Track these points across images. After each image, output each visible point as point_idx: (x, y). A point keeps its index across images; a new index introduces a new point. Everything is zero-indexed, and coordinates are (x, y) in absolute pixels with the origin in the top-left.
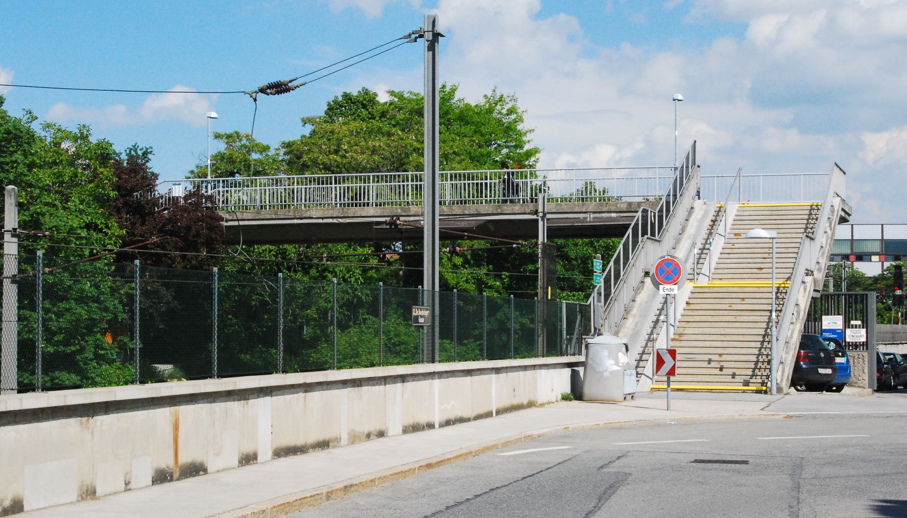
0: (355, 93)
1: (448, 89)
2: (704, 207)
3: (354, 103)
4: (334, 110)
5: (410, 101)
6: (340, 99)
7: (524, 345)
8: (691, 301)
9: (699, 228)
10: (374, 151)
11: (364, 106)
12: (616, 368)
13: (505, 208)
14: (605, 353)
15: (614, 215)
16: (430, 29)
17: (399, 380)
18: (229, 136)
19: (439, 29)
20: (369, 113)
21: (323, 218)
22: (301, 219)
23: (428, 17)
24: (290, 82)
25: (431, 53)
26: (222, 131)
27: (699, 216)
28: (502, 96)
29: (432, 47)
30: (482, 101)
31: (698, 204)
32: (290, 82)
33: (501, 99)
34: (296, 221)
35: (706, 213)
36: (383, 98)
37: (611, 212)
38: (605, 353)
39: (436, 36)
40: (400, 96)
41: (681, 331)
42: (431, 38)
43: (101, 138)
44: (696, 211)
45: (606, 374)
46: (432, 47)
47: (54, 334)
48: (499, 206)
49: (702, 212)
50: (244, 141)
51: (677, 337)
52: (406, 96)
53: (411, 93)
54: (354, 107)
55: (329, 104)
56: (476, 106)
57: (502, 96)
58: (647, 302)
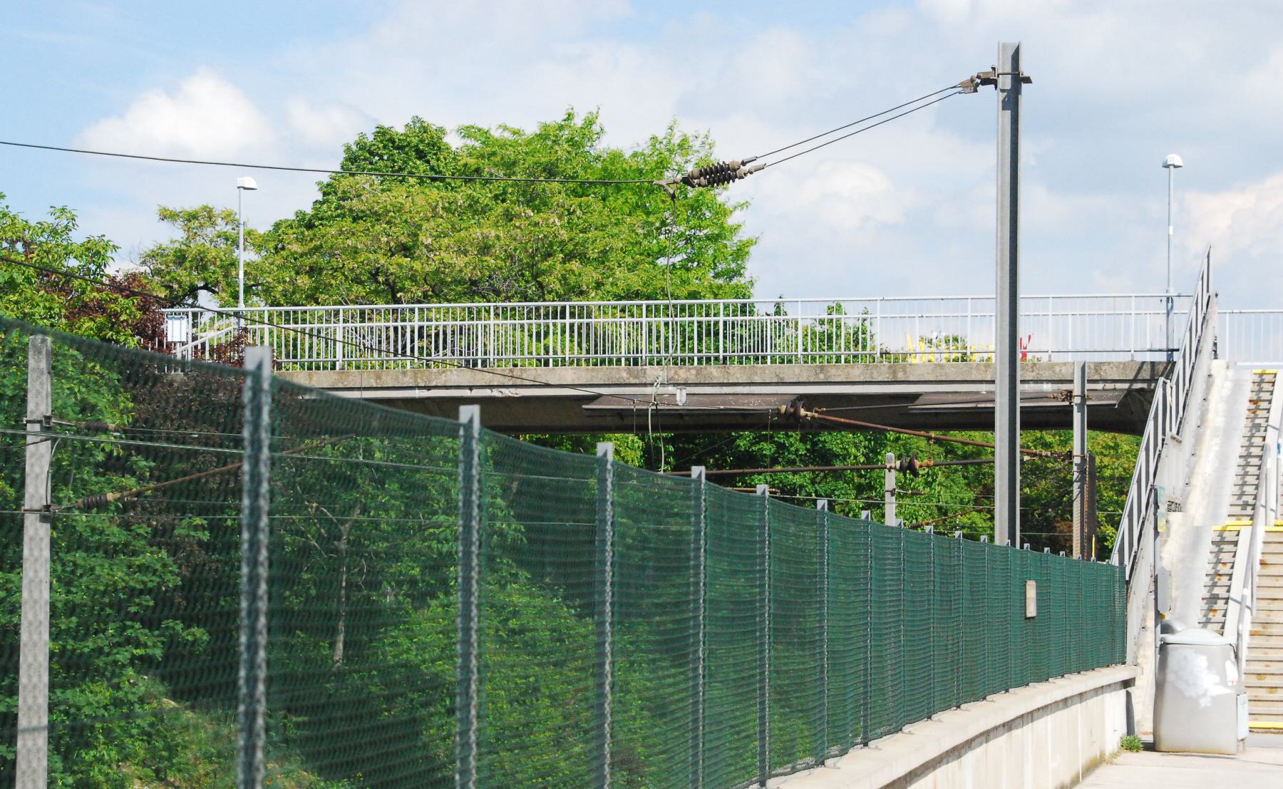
0: (400, 129)
1: (578, 122)
2: (1230, 373)
3: (398, 148)
4: (359, 158)
5: (503, 145)
6: (371, 138)
7: (22, 521)
8: (1269, 559)
9: (1230, 415)
10: (485, 249)
11: (421, 155)
12: (1222, 690)
13: (833, 371)
14: (1201, 661)
15: (1047, 387)
16: (1008, 69)
17: (983, 738)
18: (192, 217)
19: (1025, 70)
20: (432, 169)
21: (471, 388)
22: (429, 388)
23: (1004, 46)
24: (744, 163)
25: (1008, 113)
26: (175, 205)
27: (1225, 393)
28: (685, 140)
29: (1012, 102)
30: (644, 147)
31: (1217, 366)
32: (744, 163)
33: (683, 146)
34: (417, 394)
35: (1237, 385)
36: (454, 142)
37: (1041, 381)
38: (1201, 661)
39: (1019, 80)
40: (485, 136)
41: (1263, 617)
42: (1008, 86)
43: (95, 234)
44: (1218, 381)
45: (1204, 702)
46: (1012, 102)
47: (77, 631)
48: (822, 368)
49: (1229, 385)
50: (222, 227)
51: (1259, 628)
52: (496, 134)
53: (505, 128)
54: (399, 157)
55: (348, 149)
56: (635, 155)
57: (685, 140)
58: (1182, 561)
